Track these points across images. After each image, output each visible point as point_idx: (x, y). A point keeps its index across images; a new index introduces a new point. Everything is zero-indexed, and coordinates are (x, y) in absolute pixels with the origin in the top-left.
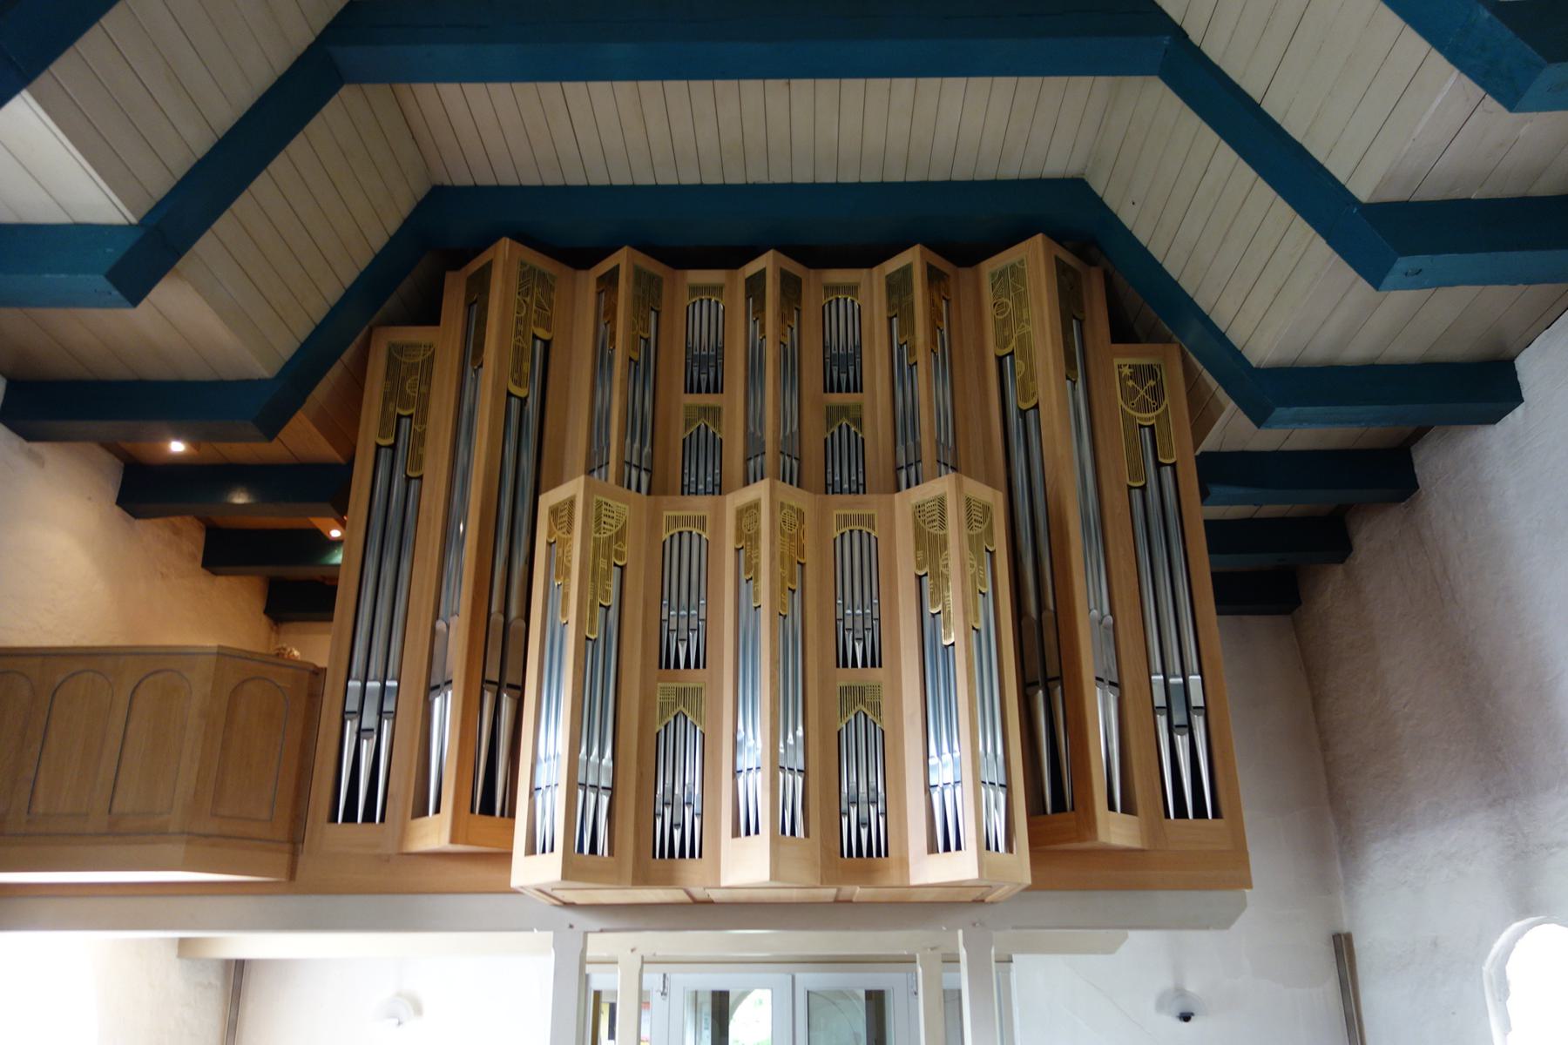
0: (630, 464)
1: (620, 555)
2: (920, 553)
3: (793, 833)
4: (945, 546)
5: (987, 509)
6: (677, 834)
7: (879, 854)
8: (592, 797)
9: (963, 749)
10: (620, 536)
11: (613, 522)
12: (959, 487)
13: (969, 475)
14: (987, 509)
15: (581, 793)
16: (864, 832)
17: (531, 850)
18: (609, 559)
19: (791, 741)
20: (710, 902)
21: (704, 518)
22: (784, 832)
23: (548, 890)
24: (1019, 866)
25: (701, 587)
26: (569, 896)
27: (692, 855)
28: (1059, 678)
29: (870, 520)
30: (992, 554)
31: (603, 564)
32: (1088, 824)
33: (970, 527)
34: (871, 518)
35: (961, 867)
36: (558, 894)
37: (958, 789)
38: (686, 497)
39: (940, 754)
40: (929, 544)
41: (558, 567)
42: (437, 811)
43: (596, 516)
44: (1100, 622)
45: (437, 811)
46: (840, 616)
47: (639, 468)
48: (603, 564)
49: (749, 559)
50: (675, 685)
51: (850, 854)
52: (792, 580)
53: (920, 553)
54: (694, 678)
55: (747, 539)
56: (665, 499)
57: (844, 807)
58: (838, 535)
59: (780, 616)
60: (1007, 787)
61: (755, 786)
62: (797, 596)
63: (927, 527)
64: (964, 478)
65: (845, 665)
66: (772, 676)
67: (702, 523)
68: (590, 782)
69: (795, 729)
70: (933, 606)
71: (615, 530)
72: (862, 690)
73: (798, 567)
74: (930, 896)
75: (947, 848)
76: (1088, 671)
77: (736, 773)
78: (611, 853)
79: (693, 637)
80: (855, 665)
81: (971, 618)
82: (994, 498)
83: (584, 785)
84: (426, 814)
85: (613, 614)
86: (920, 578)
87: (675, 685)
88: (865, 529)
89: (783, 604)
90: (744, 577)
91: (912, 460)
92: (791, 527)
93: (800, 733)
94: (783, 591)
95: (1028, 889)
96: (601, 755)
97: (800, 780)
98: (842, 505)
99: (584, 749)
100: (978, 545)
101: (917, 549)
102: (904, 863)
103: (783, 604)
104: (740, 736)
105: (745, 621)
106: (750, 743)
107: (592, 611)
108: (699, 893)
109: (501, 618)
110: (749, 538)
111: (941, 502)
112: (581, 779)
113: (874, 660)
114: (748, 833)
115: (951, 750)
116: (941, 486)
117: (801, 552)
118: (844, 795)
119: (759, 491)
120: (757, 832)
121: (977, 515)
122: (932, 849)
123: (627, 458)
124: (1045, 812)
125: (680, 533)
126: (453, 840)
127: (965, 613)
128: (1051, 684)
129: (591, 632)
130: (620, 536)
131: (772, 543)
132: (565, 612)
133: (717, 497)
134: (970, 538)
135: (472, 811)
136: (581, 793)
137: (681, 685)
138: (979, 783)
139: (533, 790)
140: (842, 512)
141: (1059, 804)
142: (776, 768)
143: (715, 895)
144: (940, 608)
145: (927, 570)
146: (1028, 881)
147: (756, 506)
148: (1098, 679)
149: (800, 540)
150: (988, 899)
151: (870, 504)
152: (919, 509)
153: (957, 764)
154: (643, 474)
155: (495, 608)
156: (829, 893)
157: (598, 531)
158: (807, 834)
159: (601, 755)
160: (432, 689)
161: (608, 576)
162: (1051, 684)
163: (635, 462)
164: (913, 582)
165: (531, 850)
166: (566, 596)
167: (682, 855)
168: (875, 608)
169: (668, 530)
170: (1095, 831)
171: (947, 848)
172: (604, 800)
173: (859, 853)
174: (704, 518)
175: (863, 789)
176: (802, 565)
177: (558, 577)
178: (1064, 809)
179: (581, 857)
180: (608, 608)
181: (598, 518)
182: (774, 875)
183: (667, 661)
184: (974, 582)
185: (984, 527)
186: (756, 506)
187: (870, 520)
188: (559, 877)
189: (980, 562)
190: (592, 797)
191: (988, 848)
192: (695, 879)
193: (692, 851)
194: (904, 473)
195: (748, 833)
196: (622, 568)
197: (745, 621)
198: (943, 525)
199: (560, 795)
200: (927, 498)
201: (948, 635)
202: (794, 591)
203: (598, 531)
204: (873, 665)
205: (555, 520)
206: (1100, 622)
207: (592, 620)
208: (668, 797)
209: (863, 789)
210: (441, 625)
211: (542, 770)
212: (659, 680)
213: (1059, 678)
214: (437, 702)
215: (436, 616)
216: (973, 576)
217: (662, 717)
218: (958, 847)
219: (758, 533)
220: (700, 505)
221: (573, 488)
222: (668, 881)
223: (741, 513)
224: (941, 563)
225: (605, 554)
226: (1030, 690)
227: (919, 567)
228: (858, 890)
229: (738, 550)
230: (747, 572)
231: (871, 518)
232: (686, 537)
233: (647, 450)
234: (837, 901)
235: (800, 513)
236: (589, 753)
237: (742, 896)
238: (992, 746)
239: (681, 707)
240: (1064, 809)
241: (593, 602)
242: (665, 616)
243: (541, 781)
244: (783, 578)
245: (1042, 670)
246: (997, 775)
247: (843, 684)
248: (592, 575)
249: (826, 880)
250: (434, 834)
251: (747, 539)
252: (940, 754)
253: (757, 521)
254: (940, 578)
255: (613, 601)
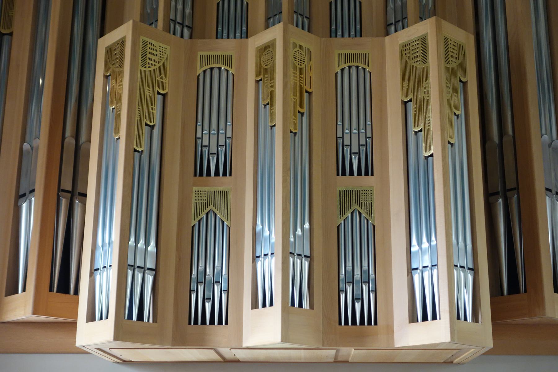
0: (174, 21)
1: (162, 85)
2: (406, 84)
3: (300, 305)
4: (426, 75)
5: (461, 48)
6: (208, 306)
7: (370, 323)
8: (139, 276)
9: (439, 240)
10: (162, 70)
11: (156, 58)
12: (439, 28)
13: (445, 19)
14: (461, 48)
15: (130, 273)
16: (358, 306)
17: (91, 317)
18: (153, 88)
19: (299, 232)
20: (238, 361)
21: (231, 57)
22: (293, 304)
23: (107, 349)
24: (484, 332)
25: (229, 109)
26: (126, 355)
27: (220, 323)
28: (516, 189)
29: (365, 58)
30: (465, 84)
31: (148, 92)
32: (538, 301)
33: (447, 60)
34: (366, 56)
35: (436, 333)
36: (114, 352)
37: (435, 272)
38: (219, 40)
39: (420, 243)
40: (413, 75)
41: (111, 98)
42: (24, 290)
43: (143, 54)
44: (550, 146)
45: (24, 290)
46: (340, 134)
47: (182, 25)
48: (148, 92)
49: (266, 89)
50: (207, 189)
51: (346, 323)
52: (301, 105)
53: (406, 84)
54: (220, 184)
55: (265, 73)
56: (199, 42)
57: (342, 285)
58: (338, 70)
59: (291, 134)
60: (474, 270)
61: (270, 268)
62: (305, 118)
63: (411, 63)
64: (443, 22)
65: (344, 174)
66: (284, 181)
67: (228, 60)
68: (139, 263)
69: (303, 223)
70: (416, 125)
71: (158, 65)
72: (357, 194)
73: (306, 95)
74: (410, 357)
75: (425, 318)
76: (540, 185)
77: (255, 258)
78: (155, 320)
79: (222, 150)
80: (351, 173)
81: (447, 134)
82: (464, 38)
83: (133, 267)
84: (17, 292)
85: (156, 132)
86: (405, 103)
87: (207, 189)
88: (361, 65)
89: (293, 124)
90: (262, 103)
91: (399, 17)
92: (299, 63)
93: (307, 226)
94: (293, 113)
95: (489, 353)
96: (147, 244)
97: (306, 264)
98: (344, 45)
99: (132, 239)
100: (453, 76)
101: (403, 80)
102: (390, 330)
103: (293, 124)
104: (259, 227)
105: (263, 144)
106: (267, 233)
107: (139, 129)
108: (228, 353)
109: (73, 142)
110: (267, 71)
111: (424, 40)
112: (130, 261)
113: (367, 170)
114: (264, 305)
115: (429, 240)
116: (425, 28)
117: (309, 83)
118: (342, 276)
119: (275, 33)
120: (271, 304)
121: (453, 52)
122: (413, 319)
123: (172, 17)
124: (502, 294)
125: (212, 69)
126: (35, 312)
127: (442, 130)
128: (509, 194)
129: (139, 145)
130: (162, 70)
131: (285, 75)
132: (117, 130)
133: (244, 40)
134: (447, 70)
135: (51, 290)
136: (130, 273)
137: (213, 189)
138: (452, 266)
139: (93, 271)
140: (343, 52)
141: (514, 288)
142: (288, 253)
143: (241, 355)
144: (422, 127)
145: (411, 96)
146: (490, 344)
147: (271, 45)
148: (547, 189)
149: (307, 73)
150: (456, 361)
151: (366, 45)
152: (405, 47)
153: (433, 251)
154: (186, 31)
155: (68, 133)
156: (329, 354)
157: (144, 65)
158: (312, 307)
159: (147, 244)
160: (20, 196)
161: (152, 102)
162: (509, 194)
163: (179, 19)
164: (399, 107)
165: (91, 317)
166: (118, 118)
167: (212, 322)
168: (369, 128)
169: (201, 67)
170: (544, 309)
171: (425, 318)
172: (150, 279)
173: (354, 322)
174: (231, 57)
175: (357, 271)
176: (310, 93)
177: (112, 103)
178: (517, 291)
179: (130, 323)
180: (152, 127)
181: (144, 55)
182: (285, 338)
183: (201, 170)
184: (450, 106)
185: (459, 62)
186: (271, 45)
187: (365, 58)
188: (112, 338)
189: (455, 90)
190: (139, 276)
191: (458, 318)
192: (221, 343)
193: (222, 320)
194: (395, 21)
195: (264, 305)
196: (164, 95)
197: (263, 144)
198: (425, 59)
199: (113, 273)
200: (412, 38)
201: (427, 148)
202: (302, 114)
203: (144, 65)
204: (367, 174)
205: (110, 58)
206: (550, 146)
207: (139, 136)
208: (201, 278)
209: (357, 271)
210: (26, 146)
211: (100, 253)
212: (195, 185)
213: (516, 189)
214: (24, 206)
215: (23, 140)
216: (449, 100)
217: (196, 214)
218: (434, 318)
219: (273, 67)
220: (227, 46)
221: (123, 32)
222: (200, 342)
223: (260, 52)
224: (423, 91)
225: (150, 87)
226: (491, 199)
227: (405, 94)
228: (353, 351)
229: (257, 82)
230: (264, 99)
231: (366, 56)
232: (216, 73)
233: (188, 11)
234: (336, 362)
235: (308, 53)
236: (137, 241)
237: (261, 355)
238: (463, 245)
239: (211, 207)
240: (517, 291)
241: (140, 122)
242: (199, 135)
243: (99, 264)
244: (293, 104)
245: (504, 186)
246: (466, 260)
247: (342, 189)
248: (139, 100)
249: (326, 343)
250: (21, 308)
251: (265, 73)
252: (420, 243)
253: (273, 57)
254: (423, 104)
255: (157, 121)
